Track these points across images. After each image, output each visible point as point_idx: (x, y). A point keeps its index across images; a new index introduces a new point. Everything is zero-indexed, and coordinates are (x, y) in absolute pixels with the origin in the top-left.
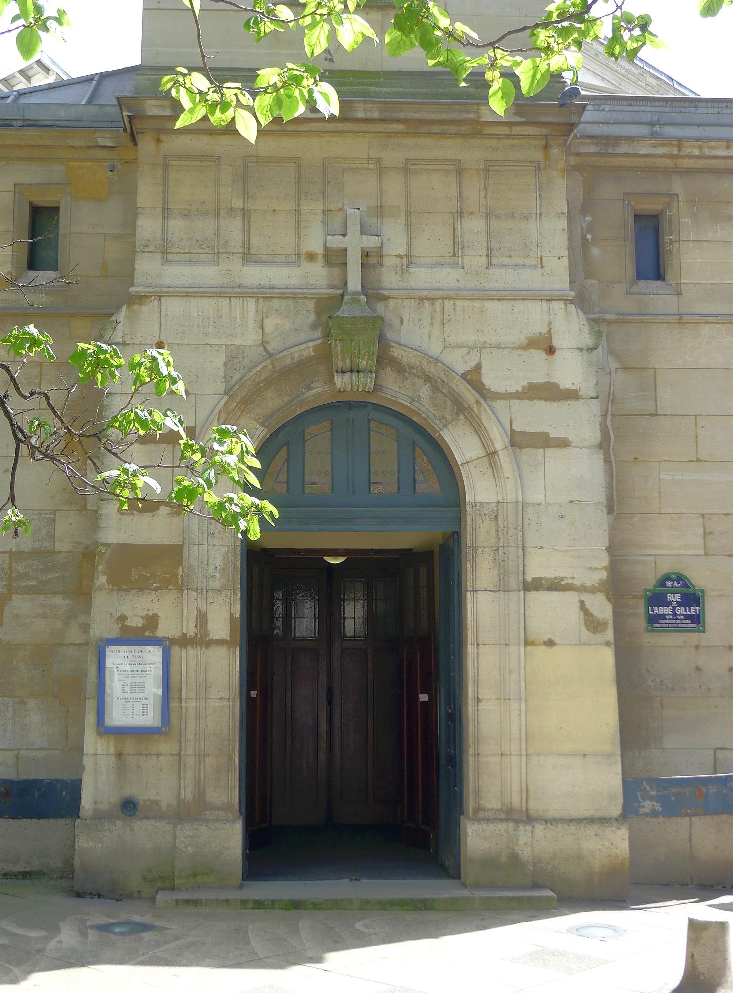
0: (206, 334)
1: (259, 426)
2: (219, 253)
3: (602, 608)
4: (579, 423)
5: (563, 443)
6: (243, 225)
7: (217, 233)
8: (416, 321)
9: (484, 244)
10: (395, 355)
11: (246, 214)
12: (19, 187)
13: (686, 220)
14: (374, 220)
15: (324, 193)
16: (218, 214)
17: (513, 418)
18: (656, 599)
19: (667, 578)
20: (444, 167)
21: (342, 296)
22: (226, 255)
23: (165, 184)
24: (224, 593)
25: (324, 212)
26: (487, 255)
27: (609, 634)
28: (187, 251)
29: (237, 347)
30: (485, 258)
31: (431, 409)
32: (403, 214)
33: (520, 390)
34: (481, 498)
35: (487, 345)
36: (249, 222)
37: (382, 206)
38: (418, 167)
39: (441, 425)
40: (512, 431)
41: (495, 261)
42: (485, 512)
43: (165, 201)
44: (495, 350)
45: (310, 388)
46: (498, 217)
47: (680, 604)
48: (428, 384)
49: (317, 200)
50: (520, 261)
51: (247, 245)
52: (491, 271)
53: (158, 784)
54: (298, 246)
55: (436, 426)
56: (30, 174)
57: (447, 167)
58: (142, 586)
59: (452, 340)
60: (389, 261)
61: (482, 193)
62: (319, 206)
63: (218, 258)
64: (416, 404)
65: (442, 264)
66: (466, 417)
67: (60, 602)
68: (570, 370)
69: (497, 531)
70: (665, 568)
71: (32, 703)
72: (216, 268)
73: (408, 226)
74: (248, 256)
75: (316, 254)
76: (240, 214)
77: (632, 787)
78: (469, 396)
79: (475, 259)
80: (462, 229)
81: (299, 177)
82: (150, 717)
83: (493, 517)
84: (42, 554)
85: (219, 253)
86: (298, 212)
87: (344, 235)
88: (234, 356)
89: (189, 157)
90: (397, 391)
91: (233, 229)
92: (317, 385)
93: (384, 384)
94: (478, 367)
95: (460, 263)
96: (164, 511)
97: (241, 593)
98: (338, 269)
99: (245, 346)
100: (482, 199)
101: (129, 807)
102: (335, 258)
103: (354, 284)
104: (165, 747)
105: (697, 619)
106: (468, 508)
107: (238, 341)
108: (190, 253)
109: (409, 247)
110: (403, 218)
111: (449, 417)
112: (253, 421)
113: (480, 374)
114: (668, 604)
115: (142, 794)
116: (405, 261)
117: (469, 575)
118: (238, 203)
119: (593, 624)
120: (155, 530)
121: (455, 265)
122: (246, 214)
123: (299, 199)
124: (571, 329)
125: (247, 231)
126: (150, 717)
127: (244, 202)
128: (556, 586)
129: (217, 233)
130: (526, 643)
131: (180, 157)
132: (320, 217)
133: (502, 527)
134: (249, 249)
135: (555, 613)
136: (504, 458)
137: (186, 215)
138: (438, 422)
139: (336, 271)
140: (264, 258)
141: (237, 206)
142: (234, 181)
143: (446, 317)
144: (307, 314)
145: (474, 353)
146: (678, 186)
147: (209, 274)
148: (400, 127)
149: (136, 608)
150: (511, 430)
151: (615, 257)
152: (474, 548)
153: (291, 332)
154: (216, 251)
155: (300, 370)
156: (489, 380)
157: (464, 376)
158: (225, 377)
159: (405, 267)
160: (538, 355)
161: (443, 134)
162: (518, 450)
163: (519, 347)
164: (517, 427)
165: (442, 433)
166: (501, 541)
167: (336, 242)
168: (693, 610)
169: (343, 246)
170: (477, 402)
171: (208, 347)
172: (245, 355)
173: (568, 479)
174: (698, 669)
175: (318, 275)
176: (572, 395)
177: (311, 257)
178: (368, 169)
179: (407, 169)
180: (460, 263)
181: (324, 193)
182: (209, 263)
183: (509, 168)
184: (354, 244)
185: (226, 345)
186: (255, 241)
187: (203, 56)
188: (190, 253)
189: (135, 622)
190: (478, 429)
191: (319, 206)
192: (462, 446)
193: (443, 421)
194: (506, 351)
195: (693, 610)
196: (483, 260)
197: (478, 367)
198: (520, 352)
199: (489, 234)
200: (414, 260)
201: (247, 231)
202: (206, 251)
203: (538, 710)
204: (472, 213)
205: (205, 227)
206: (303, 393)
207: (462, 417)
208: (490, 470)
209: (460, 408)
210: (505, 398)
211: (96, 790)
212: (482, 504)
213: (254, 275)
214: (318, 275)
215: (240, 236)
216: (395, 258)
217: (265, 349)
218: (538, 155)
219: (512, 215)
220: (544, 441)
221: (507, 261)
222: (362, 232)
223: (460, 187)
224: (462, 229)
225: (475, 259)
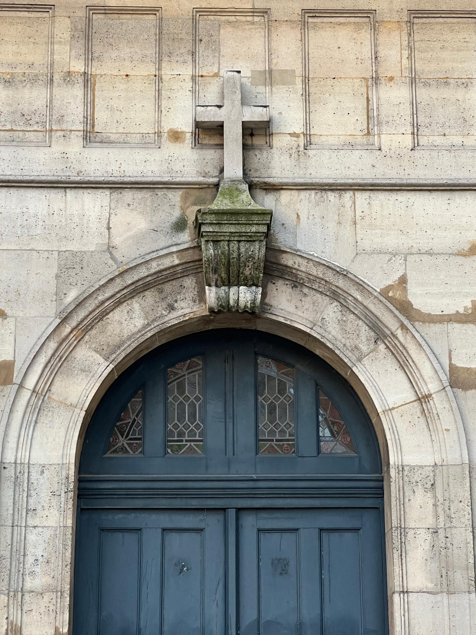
0: (32, 237)
1: (101, 360)
2: (51, 130)
6: (85, 95)
7: (50, 105)
8: (318, 220)
9: (409, 119)
10: (290, 263)
11: (88, 81)
14: (261, 89)
15: (193, 54)
16: (52, 80)
17: (453, 347)
20: (353, 20)
21: (217, 186)
22: (62, 133)
24: (47, 597)
25: (194, 78)
26: (413, 134)
28: (8, 127)
29: (74, 254)
30: (410, 137)
31: (340, 337)
32: (299, 81)
33: (461, 311)
34: (410, 459)
35: (414, 251)
36: (93, 91)
37: (271, 71)
38: (319, 20)
39: (354, 359)
40: (452, 368)
41: (423, 141)
42: (416, 478)
44: (425, 258)
45: (171, 308)
46: (426, 84)
48: (336, 303)
49: (185, 62)
50: (457, 140)
51: (89, 120)
52: (416, 154)
54: (159, 122)
55: (346, 360)
57: (358, 20)
59: (366, 244)
61: (406, 53)
62: (187, 71)
63: (50, 137)
64: (319, 330)
65: (352, 146)
66: (387, 347)
69: (435, 505)
72: (46, 150)
73: (307, 96)
74: (90, 136)
75: (182, 133)
76: (81, 80)
79: (396, 138)
80: (378, 99)
81: (160, 33)
83: (429, 486)
85: (51, 130)
86: (159, 78)
87: (220, 107)
88: (70, 264)
90: (290, 309)
91: (71, 100)
92: (183, 304)
93: (274, 303)
94: (403, 281)
95: (377, 144)
97: (72, 549)
98: (212, 151)
99: (85, 252)
100: (405, 61)
102: (207, 133)
103: (234, 169)
106: (393, 472)
107: (74, 246)
108: (12, 130)
109: (307, 124)
110: (299, 86)
111: (364, 348)
112: (94, 354)
113: (405, 289)
116: (302, 141)
117: (397, 569)
118: (78, 66)
121: (369, 147)
122: (88, 81)
123: (160, 61)
125: (90, 103)
127: (86, 65)
129: (50, 105)
132: (189, 85)
133: (441, 500)
134: (93, 126)
136: (439, 404)
138: (350, 354)
139: (211, 155)
140: (113, 137)
141: (76, 69)
142: (73, 37)
143: (358, 213)
144: (173, 206)
145: (399, 260)
150: (451, 365)
152: (403, 530)
153: (139, 231)
154: (49, 128)
155: (160, 281)
156: (419, 299)
157: (385, 292)
158: (56, 295)
159: (302, 149)
162: (459, 392)
163: (460, 254)
164: (459, 363)
165: (354, 369)
166: (441, 519)
167: (210, 115)
169: (218, 119)
170: (403, 327)
171: (35, 253)
172: (85, 265)
177: (176, 136)
178: (253, 23)
180: (377, 144)
181: (193, 54)
183: (441, 20)
185: (59, 252)
186: (101, 116)
187: (150, 528)
188: (12, 130)
190: (404, 363)
191: (187, 71)
193: (356, 353)
194: (441, 259)
196: (408, 141)
197: (403, 281)
198: (460, 260)
200: (314, 139)
201: (90, 103)
202: (35, 128)
204: (391, 79)
206: (162, 316)
207: (382, 347)
208: (422, 420)
209: (380, 334)
210: (441, 322)
212: (412, 468)
213: (99, 163)
214: (187, 163)
215: (81, 109)
216: (289, 137)
217: (113, 258)
219: (445, 82)
221: (439, 140)
222: (244, 102)
223: (376, 46)
224: (378, 99)
225: (396, 138)
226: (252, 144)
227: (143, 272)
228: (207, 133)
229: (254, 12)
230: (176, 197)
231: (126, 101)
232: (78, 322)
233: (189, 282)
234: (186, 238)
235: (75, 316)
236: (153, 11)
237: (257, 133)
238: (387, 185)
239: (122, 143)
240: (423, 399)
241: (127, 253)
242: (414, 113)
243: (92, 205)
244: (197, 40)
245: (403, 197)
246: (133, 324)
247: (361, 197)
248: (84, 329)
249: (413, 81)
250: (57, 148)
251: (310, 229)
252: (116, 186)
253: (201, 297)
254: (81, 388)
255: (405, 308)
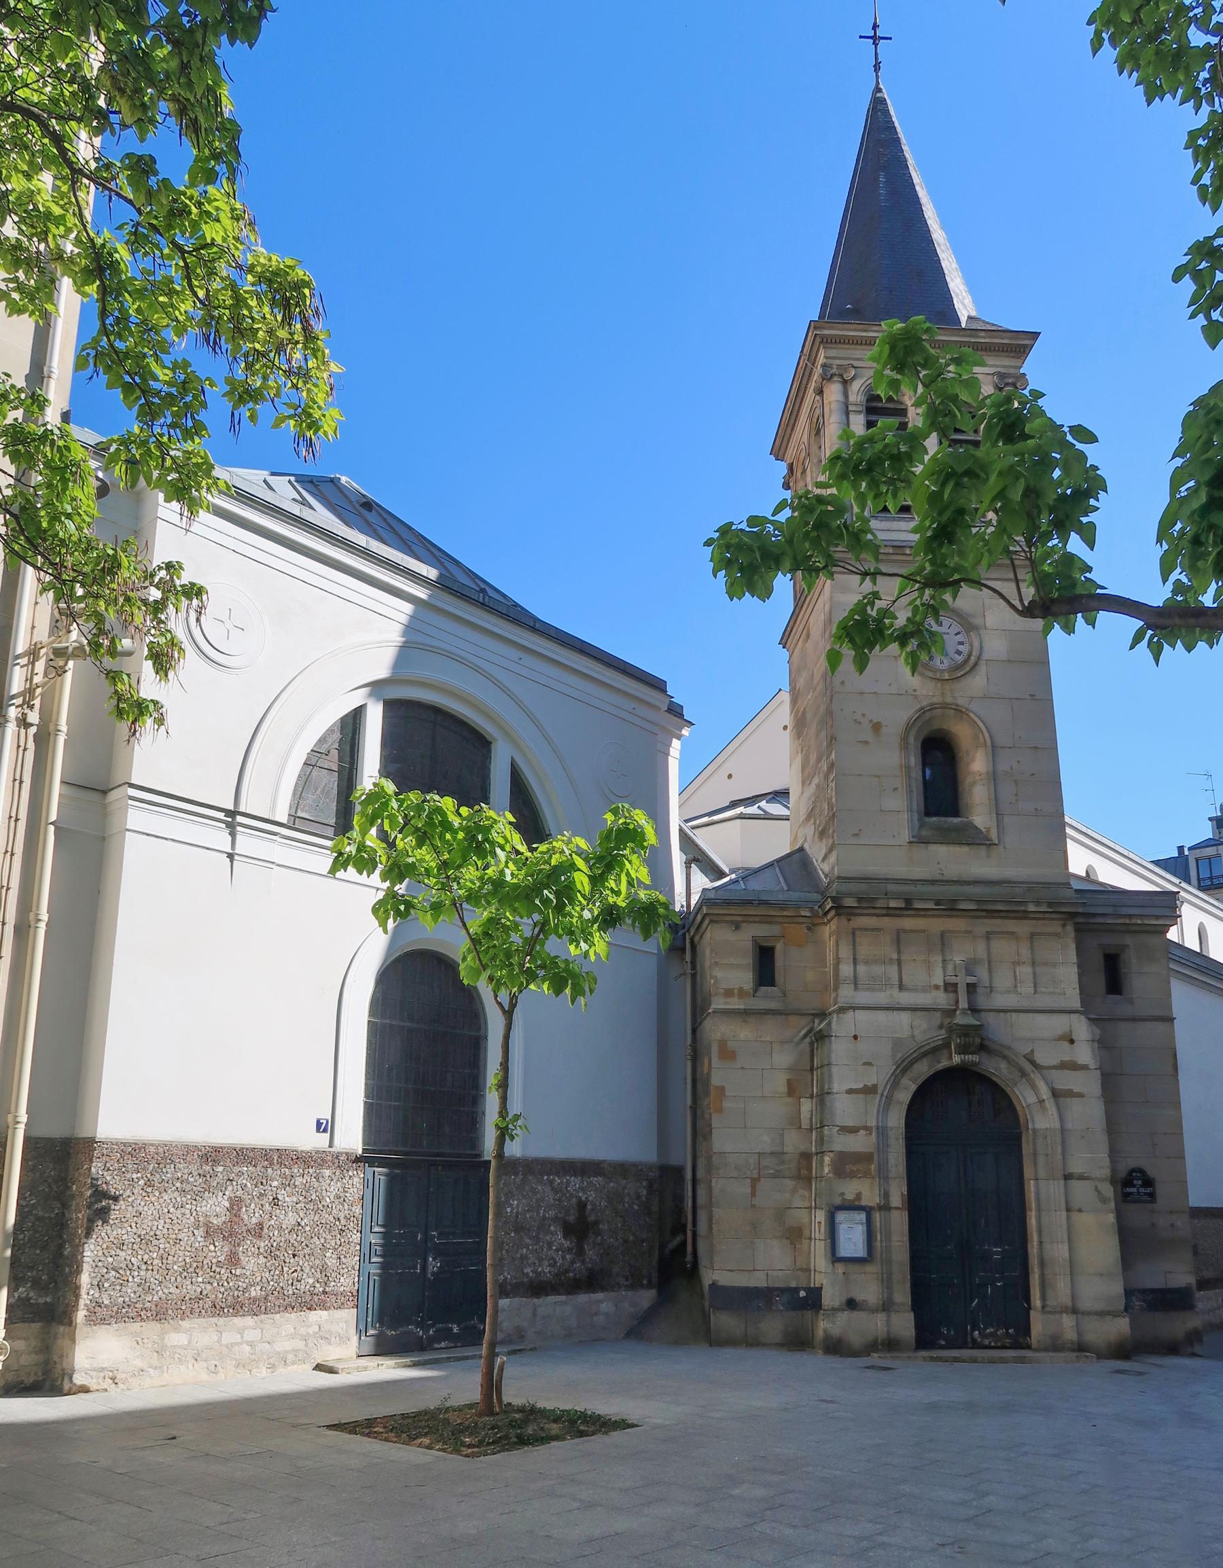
3: (1108, 1190)
4: (1089, 1084)
5: (1080, 1095)
11: (899, 962)
12: (755, 940)
13: (1134, 961)
18: (1127, 1182)
19: (1133, 1171)
21: (955, 1010)
23: (854, 946)
27: (1112, 1205)
43: (854, 955)
47: (1142, 1186)
51: (901, 980)
53: (869, 1292)
56: (761, 930)
58: (852, 1175)
60: (980, 990)
65: (1009, 992)
67: (790, 1183)
68: (1084, 1054)
70: (1132, 1163)
71: (775, 1243)
74: (901, 987)
77: (1129, 1293)
78: (1028, 1067)
79: (1027, 988)
82: (841, 1216)
84: (779, 1155)
88: (897, 1043)
89: (866, 929)
91: (893, 971)
94: (1032, 1051)
96: (862, 1132)
101: (851, 1304)
102: (950, 987)
103: (963, 1004)
104: (869, 1268)
105: (1152, 1195)
114: (1134, 1186)
115: (859, 1296)
119: (1104, 1200)
120: (859, 1143)
121: (1016, 992)
122: (899, 962)
124: (1082, 1029)
125: (79, 652)
126: (841, 1216)
128: (1081, 1177)
130: (1068, 1210)
131: (860, 929)
135: (1082, 1192)
137: (866, 962)
139: (952, 995)
144: (937, 1018)
146: (1129, 940)
147: (881, 998)
148: (984, 914)
149: (850, 1189)
151: (1100, 982)
153: (924, 1030)
155: (932, 1052)
156: (1040, 1058)
160: (1066, 1044)
161: (1007, 918)
167: (953, 980)
168: (1149, 1190)
173: (1088, 1113)
174: (1153, 1225)
175: (941, 999)
176: (1085, 1067)
177: (937, 987)
179: (988, 936)
182: (881, 990)
184: (962, 980)
189: (850, 1196)
192: (1025, 1096)
195: (1149, 1190)
197: (1032, 1051)
199: (1034, 974)
201: (79, 652)
203: (1075, 1250)
205: (878, 970)
209: (1023, 1074)
211: (830, 1298)
213: (906, 998)
214: (941, 999)
218: (1059, 930)
219: (1046, 964)
220: (1071, 1094)
226: (943, 485)
227: (928, 1047)
228: (950, 987)
229: (966, 932)
230: (938, 1014)
231: (914, 973)
232: (903, 1068)
233: (945, 1052)
234: (943, 1032)
235: (567, 1244)
236: (924, 931)
237: (972, 988)
238: (700, 1123)
239: (914, 990)
240: (1042, 1101)
241: (920, 1037)
242: (1035, 978)
243: (905, 1017)
244: (943, 944)
245: (1031, 1015)
246: (924, 1069)
247: (1014, 1015)
248: (904, 1071)
249: (1034, 964)
250: (888, 993)
251: (997, 1028)
252: (913, 1009)
253: (950, 1058)
254: (904, 1096)
255: (1033, 1063)
